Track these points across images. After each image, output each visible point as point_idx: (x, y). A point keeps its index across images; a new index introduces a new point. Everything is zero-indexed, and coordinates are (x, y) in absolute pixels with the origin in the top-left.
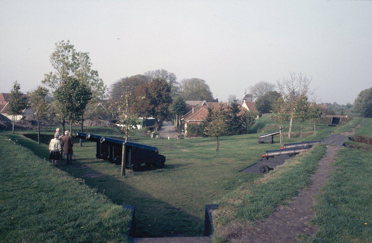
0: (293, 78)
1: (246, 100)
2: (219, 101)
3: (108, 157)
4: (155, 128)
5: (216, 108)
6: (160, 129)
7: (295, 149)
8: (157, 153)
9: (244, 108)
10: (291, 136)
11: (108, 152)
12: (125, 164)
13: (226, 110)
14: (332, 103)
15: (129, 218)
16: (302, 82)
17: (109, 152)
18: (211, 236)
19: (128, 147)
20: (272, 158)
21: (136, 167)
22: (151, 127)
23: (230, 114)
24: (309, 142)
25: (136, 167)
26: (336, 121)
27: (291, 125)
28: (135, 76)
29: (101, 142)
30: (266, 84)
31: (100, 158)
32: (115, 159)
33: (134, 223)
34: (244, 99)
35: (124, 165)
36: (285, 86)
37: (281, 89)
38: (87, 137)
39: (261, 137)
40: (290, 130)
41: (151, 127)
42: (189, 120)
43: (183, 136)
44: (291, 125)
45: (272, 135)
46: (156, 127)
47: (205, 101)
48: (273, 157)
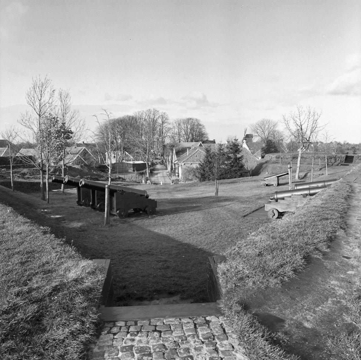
0: (300, 113)
1: (246, 140)
2: (217, 142)
3: (91, 203)
4: (146, 173)
5: (215, 149)
6: (152, 173)
7: (309, 189)
8: (147, 197)
9: (245, 148)
10: (299, 178)
11: (90, 197)
12: (109, 211)
13: (226, 150)
14: (342, 143)
15: (101, 277)
16: (310, 117)
17: (91, 198)
18: (218, 301)
19: (112, 192)
20: (282, 200)
21: (122, 213)
22: (141, 172)
23: (230, 155)
24: (324, 182)
25: (122, 213)
26: (349, 160)
27: (298, 165)
28: (123, 117)
29: (80, 185)
30: (269, 122)
31: (81, 205)
32: (98, 206)
33: (109, 285)
34: (244, 139)
35: (107, 212)
36: (292, 121)
37: (101, 339)
38: (64, 181)
39: (265, 179)
40: (298, 171)
41: (141, 172)
42: (184, 163)
43: (178, 180)
44: (298, 165)
45: (278, 177)
46: (147, 172)
47: (201, 142)
48: (283, 199)
